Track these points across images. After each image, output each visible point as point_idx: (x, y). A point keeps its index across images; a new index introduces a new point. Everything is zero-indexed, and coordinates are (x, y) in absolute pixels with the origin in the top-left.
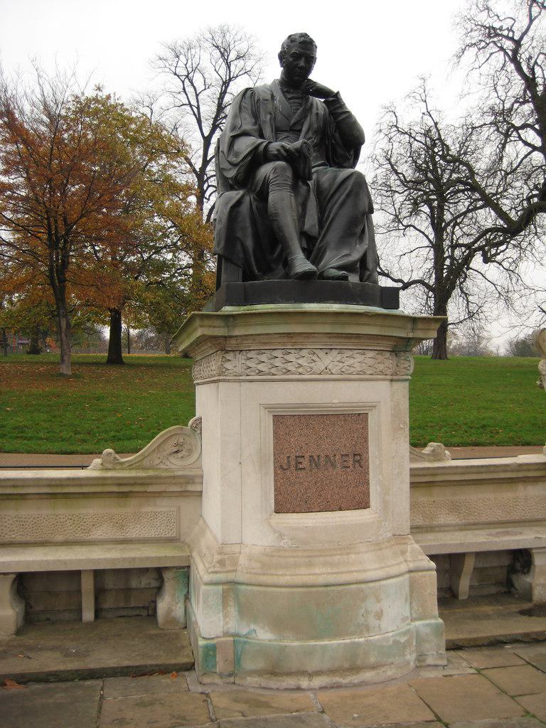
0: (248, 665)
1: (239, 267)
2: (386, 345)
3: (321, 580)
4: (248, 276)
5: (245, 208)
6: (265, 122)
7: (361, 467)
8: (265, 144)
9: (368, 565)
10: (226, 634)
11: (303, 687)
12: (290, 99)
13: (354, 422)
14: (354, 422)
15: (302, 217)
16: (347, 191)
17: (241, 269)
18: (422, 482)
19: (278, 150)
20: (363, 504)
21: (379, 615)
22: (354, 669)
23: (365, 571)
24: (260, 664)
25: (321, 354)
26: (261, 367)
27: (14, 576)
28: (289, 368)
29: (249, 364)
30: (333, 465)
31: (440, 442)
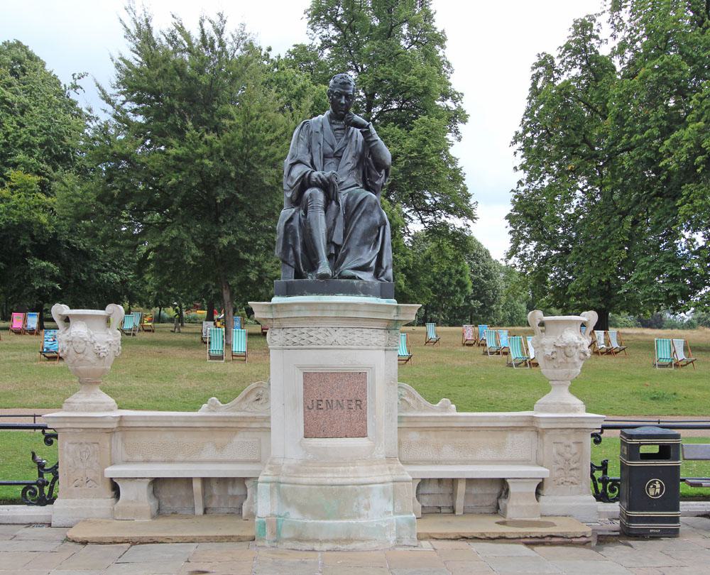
0: (285, 535)
1: (292, 267)
2: (383, 325)
3: (329, 481)
4: (298, 275)
5: (295, 223)
6: (315, 151)
7: (361, 409)
8: (309, 172)
9: (363, 474)
10: (272, 515)
11: (316, 549)
12: (335, 130)
13: (358, 378)
14: (358, 378)
15: (330, 232)
16: (362, 210)
17: (293, 269)
18: (406, 425)
19: (316, 179)
20: (363, 434)
21: (368, 507)
22: (349, 540)
23: (359, 477)
24: (291, 535)
25: (332, 331)
26: (295, 340)
27: (149, 480)
28: (311, 341)
29: (288, 337)
30: (343, 408)
31: (442, 398)
